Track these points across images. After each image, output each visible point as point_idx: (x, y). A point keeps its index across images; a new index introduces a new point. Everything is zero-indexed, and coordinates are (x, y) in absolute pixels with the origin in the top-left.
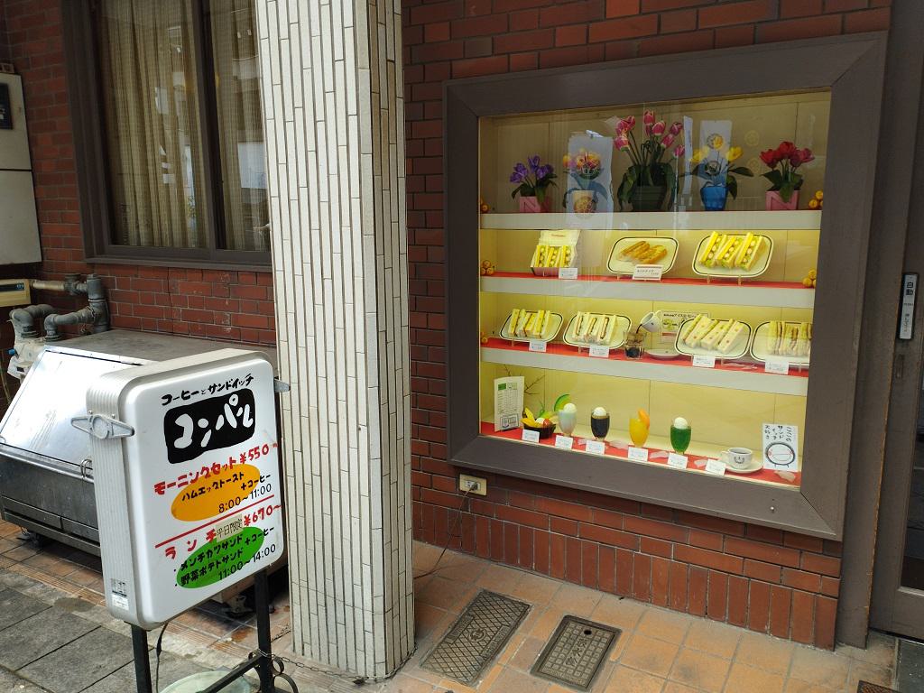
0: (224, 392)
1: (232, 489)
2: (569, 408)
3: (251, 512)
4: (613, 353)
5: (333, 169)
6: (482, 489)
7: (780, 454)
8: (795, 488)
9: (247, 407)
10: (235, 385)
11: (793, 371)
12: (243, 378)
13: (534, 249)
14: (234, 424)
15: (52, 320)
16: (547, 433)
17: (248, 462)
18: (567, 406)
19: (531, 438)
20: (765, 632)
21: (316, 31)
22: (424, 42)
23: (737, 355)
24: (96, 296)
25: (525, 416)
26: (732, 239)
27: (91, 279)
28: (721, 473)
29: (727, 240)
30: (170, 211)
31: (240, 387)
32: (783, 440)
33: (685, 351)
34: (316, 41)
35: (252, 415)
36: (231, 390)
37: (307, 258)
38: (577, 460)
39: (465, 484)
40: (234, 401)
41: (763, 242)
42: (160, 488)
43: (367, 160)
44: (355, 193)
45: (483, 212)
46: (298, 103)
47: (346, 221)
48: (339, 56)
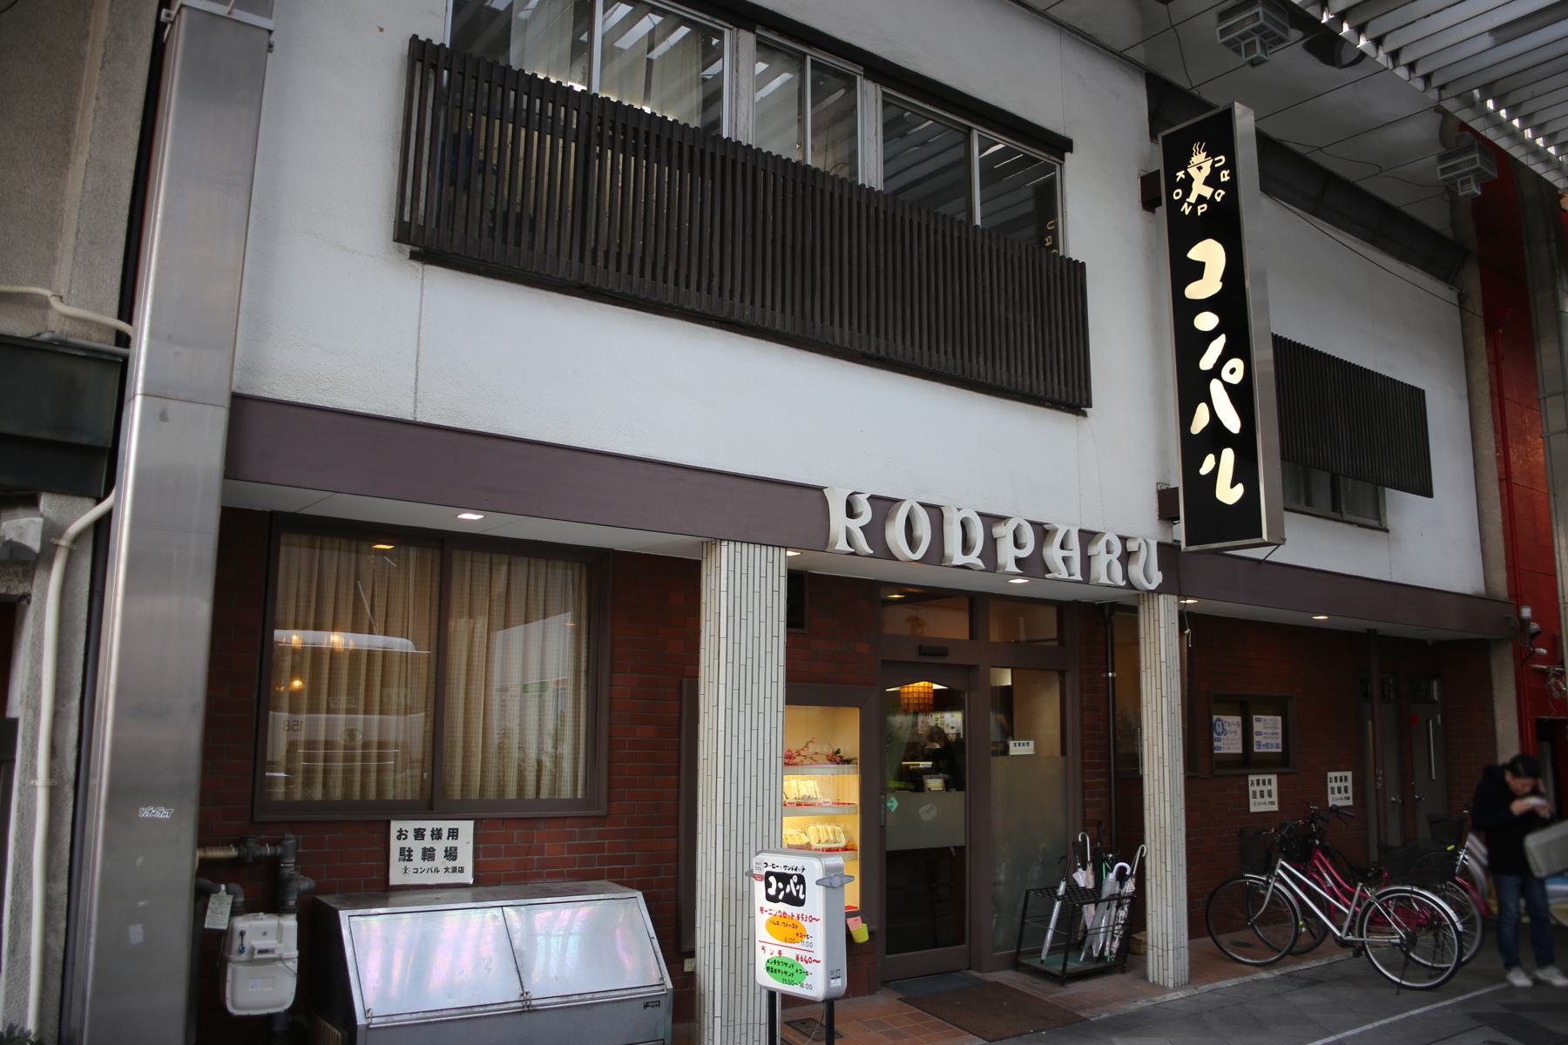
0: (790, 872)
8: (860, 183)
10: (796, 870)
12: (800, 868)
17: (800, 961)
18: (615, 101)
21: (766, 787)
22: (663, 1040)
31: (798, 872)
34: (766, 793)
35: (804, 893)
36: (794, 872)
40: (795, 879)
46: (761, 710)
48: (761, 716)
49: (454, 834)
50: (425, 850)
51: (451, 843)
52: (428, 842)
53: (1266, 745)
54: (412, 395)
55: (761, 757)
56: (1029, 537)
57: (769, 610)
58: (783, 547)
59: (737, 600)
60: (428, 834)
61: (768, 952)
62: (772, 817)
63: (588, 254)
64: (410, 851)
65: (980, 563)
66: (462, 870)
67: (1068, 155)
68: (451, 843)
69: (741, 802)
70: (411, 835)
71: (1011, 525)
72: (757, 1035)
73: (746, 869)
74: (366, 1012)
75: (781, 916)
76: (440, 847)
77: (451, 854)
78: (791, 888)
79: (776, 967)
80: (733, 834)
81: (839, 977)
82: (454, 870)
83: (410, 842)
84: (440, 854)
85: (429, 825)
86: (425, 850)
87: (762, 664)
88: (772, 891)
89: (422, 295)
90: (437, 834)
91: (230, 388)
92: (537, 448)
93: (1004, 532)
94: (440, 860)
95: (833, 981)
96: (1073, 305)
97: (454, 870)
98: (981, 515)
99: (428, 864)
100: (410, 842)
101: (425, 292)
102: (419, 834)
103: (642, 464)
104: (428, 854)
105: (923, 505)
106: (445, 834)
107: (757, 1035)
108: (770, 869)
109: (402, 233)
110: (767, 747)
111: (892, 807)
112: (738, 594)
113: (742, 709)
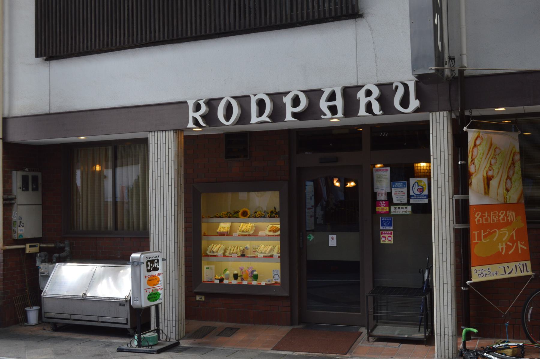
1: (155, 281)
2: (228, 272)
3: (158, 288)
4: (238, 257)
5: (168, 209)
6: (203, 299)
7: (276, 277)
9: (158, 263)
12: (157, 256)
13: (218, 227)
14: (156, 267)
15: (56, 256)
16: (221, 280)
19: (217, 282)
20: (276, 325)
24: (68, 248)
25: (215, 276)
26: (246, 225)
27: (67, 242)
28: (264, 284)
29: (245, 225)
30: (83, 218)
32: (277, 273)
35: (159, 265)
36: (156, 258)
37: (160, 230)
38: (230, 285)
39: (198, 298)
40: (156, 261)
41: (252, 225)
42: (145, 277)
43: (176, 207)
44: (173, 214)
45: (203, 218)
47: (170, 221)
54: (49, 105)
56: (303, 98)
58: (167, 130)
61: (148, 292)
62: (171, 239)
65: (268, 120)
69: (157, 233)
72: (166, 324)
75: (152, 277)
78: (155, 265)
79: (150, 297)
80: (155, 245)
81: (138, 300)
87: (165, 179)
88: (149, 268)
89: (50, 71)
91: (3, 114)
92: (81, 113)
93: (287, 100)
95: (135, 301)
98: (268, 95)
101: (50, 70)
107: (166, 324)
108: (148, 259)
110: (168, 211)
111: (310, 239)
113: (157, 197)
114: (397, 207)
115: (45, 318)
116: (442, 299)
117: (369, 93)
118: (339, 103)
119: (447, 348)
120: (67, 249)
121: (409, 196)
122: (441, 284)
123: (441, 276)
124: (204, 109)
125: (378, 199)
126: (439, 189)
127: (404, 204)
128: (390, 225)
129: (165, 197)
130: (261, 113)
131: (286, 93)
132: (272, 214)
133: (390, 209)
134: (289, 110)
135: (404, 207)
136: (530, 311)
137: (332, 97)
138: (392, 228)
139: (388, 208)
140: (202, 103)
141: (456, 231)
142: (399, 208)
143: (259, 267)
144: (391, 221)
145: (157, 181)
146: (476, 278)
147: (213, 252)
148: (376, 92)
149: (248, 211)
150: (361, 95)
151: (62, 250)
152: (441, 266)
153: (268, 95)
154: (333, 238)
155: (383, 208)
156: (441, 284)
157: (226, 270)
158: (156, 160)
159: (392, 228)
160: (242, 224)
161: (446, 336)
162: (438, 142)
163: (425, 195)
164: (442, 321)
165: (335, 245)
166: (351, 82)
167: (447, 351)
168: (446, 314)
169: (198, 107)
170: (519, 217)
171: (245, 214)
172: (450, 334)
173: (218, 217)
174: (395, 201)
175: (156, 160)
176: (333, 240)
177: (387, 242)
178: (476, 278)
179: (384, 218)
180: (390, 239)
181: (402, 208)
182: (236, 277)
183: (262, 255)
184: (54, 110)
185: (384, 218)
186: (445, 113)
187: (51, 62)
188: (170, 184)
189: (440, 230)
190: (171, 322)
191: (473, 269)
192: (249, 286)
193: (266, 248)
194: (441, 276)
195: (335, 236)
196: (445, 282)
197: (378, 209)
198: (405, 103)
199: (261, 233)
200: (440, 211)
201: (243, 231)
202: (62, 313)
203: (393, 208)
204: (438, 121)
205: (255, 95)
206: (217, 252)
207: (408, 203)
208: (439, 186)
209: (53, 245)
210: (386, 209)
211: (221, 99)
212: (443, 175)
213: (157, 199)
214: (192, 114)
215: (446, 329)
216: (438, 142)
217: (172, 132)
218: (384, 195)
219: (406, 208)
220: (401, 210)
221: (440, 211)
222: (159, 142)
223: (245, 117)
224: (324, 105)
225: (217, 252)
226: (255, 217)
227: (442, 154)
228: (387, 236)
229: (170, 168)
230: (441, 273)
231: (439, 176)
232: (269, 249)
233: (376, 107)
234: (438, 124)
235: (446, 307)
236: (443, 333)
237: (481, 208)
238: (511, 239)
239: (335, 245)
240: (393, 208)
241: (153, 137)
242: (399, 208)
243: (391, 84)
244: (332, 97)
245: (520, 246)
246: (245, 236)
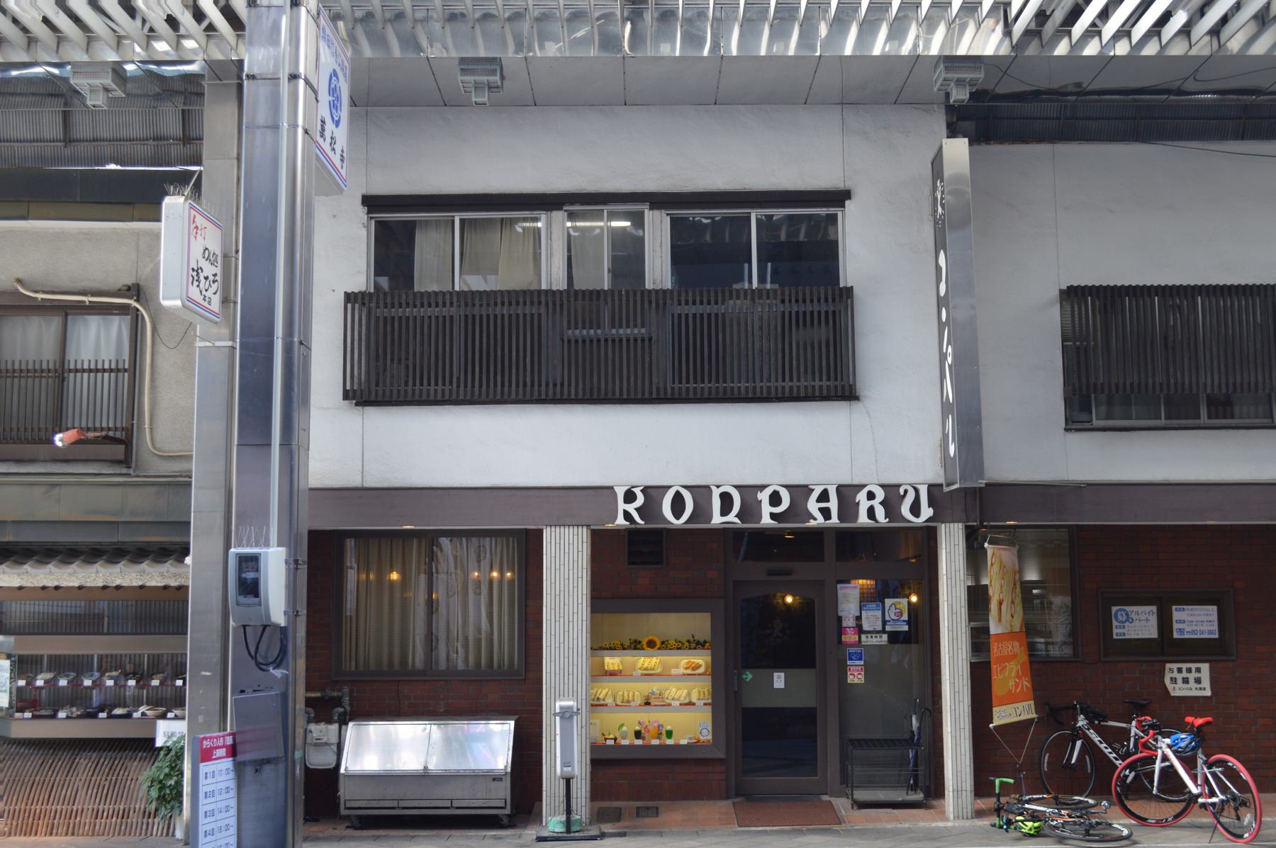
2: (624, 728)
5: (575, 637)
7: (705, 732)
11: (705, 704)
23: (687, 701)
33: (668, 701)
34: (567, 555)
47: (580, 654)
49: (1198, 670)
50: (1183, 678)
51: (1198, 675)
52: (1185, 674)
53: (1193, 632)
55: (571, 646)
57: (575, 563)
59: (553, 559)
60: (1184, 670)
63: (455, 380)
64: (1176, 679)
65: (737, 520)
66: (1204, 689)
67: (847, 203)
68: (1198, 675)
70: (1175, 670)
71: (768, 491)
73: (553, 712)
74: (346, 768)
76: (1191, 677)
77: (1198, 681)
80: (553, 690)
82: (1200, 689)
83: (1175, 674)
84: (1192, 681)
85: (1184, 666)
86: (1183, 678)
87: (571, 594)
90: (1189, 670)
93: (764, 497)
94: (1192, 684)
96: (514, 338)
97: (1200, 689)
98: (736, 487)
99: (1185, 686)
100: (1175, 674)
102: (1180, 670)
103: (487, 491)
104: (1186, 681)
105: (685, 487)
106: (1193, 670)
109: (347, 395)
112: (553, 555)
113: (557, 619)
114: (869, 635)
115: (345, 808)
116: (958, 747)
117: (871, 496)
118: (833, 505)
119: (964, 806)
120: (346, 700)
121: (884, 623)
122: (958, 729)
123: (957, 720)
124: (640, 500)
125: (844, 624)
126: (954, 616)
127: (878, 632)
128: (860, 659)
129: (571, 620)
130: (726, 510)
131: (763, 487)
132: (696, 644)
133: (860, 638)
134: (767, 509)
135: (878, 635)
136: (1047, 757)
137: (824, 497)
138: (862, 663)
139: (857, 636)
140: (637, 491)
141: (973, 665)
142: (872, 637)
143: (668, 719)
144: (861, 653)
145: (557, 597)
146: (997, 721)
147: (598, 699)
148: (880, 495)
149: (655, 639)
150: (862, 497)
151: (337, 702)
152: (957, 708)
153: (736, 487)
154: (779, 677)
155: (851, 637)
156: (958, 729)
157: (622, 725)
158: (558, 567)
159: (862, 663)
160: (643, 658)
161: (964, 792)
162: (953, 560)
163: (904, 621)
164: (959, 774)
165: (783, 687)
166: (846, 480)
167: (965, 810)
168: (963, 766)
169: (630, 497)
170: (1023, 648)
171: (651, 644)
172: (969, 789)
173: (607, 649)
174: (866, 627)
175: (558, 567)
176: (779, 680)
177: (856, 681)
178: (997, 721)
179: (852, 650)
180: (860, 676)
181: (876, 637)
182: (638, 735)
183: (677, 703)
184: (370, 483)
185: (852, 650)
186: (960, 525)
187: (366, 408)
188: (580, 601)
189: (956, 664)
190: (579, 800)
191: (994, 709)
192: (662, 747)
193: (679, 693)
194: (957, 720)
195: (782, 675)
196: (962, 727)
197: (844, 638)
198: (915, 510)
199: (674, 671)
200: (955, 641)
201: (646, 669)
202: (381, 798)
203: (863, 637)
204: (952, 534)
205: (718, 487)
206: (604, 700)
207: (884, 631)
208: (954, 611)
209: (318, 695)
210: (855, 638)
211: (670, 487)
212: (958, 599)
213: (557, 623)
214: (622, 506)
215: (964, 784)
216: (953, 560)
217: (585, 529)
218: (851, 619)
219: (881, 637)
220: (874, 640)
221: (955, 641)
222: (562, 541)
223: (702, 512)
224: (813, 506)
225: (604, 700)
226: (690, 649)
227: (958, 573)
228: (856, 673)
229: (580, 580)
230: (957, 716)
231: (954, 599)
232: (684, 694)
233: (880, 513)
234: (952, 538)
235: (963, 757)
236: (960, 789)
237: (1000, 637)
238: (1018, 676)
239: (783, 687)
240: (863, 637)
241: (553, 534)
242: (872, 637)
243: (899, 486)
244: (824, 497)
245: (1025, 682)
246: (648, 675)
